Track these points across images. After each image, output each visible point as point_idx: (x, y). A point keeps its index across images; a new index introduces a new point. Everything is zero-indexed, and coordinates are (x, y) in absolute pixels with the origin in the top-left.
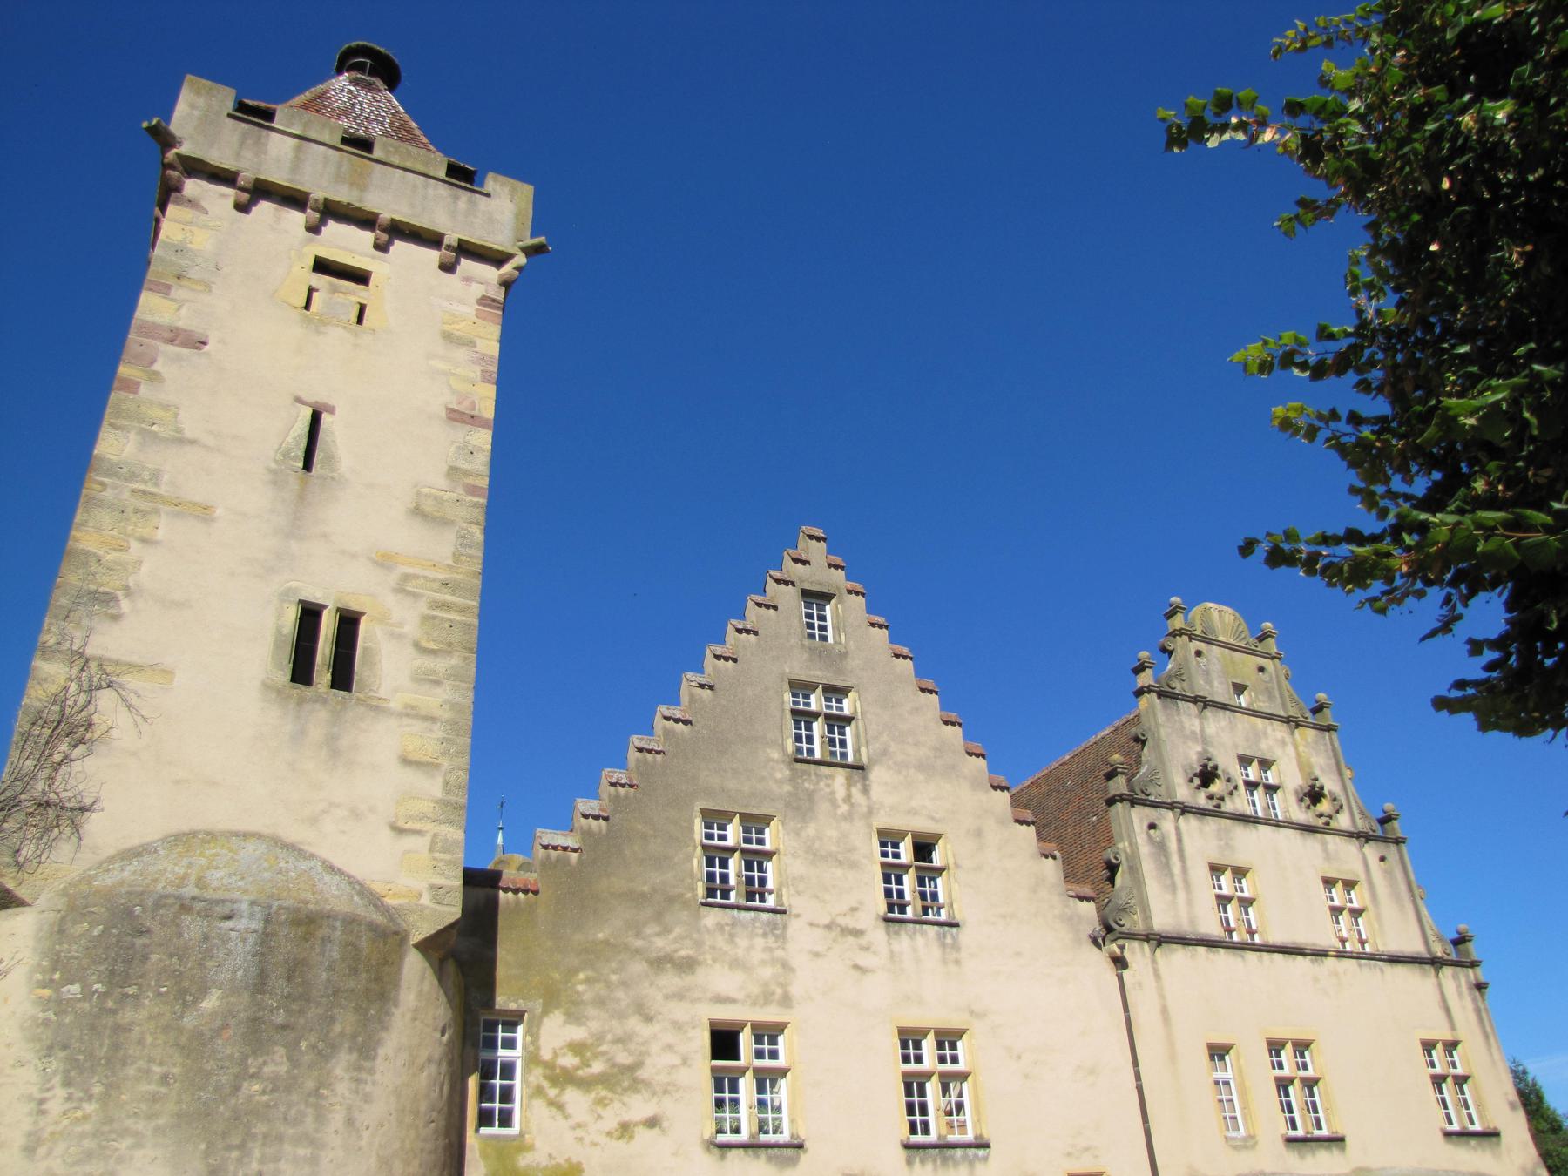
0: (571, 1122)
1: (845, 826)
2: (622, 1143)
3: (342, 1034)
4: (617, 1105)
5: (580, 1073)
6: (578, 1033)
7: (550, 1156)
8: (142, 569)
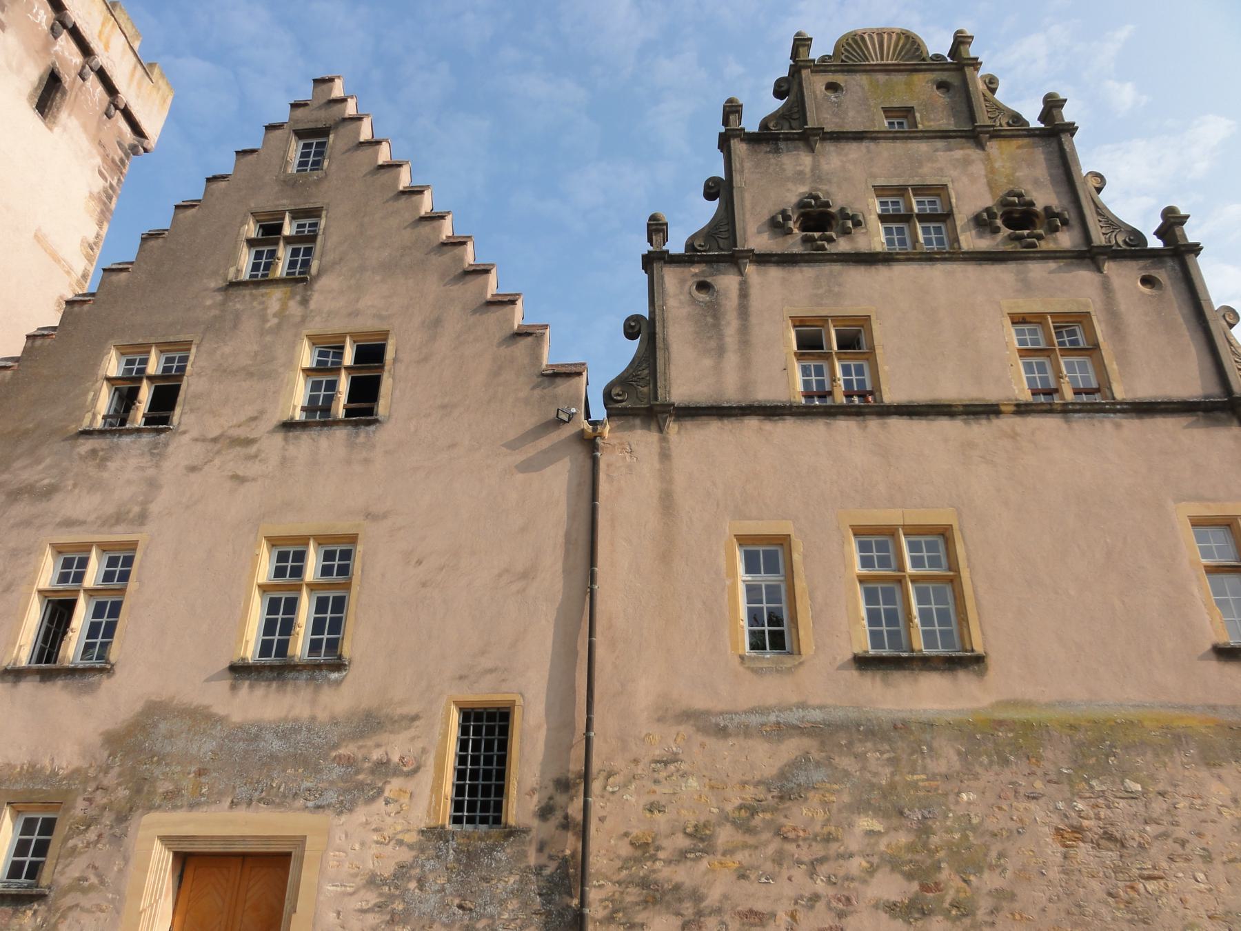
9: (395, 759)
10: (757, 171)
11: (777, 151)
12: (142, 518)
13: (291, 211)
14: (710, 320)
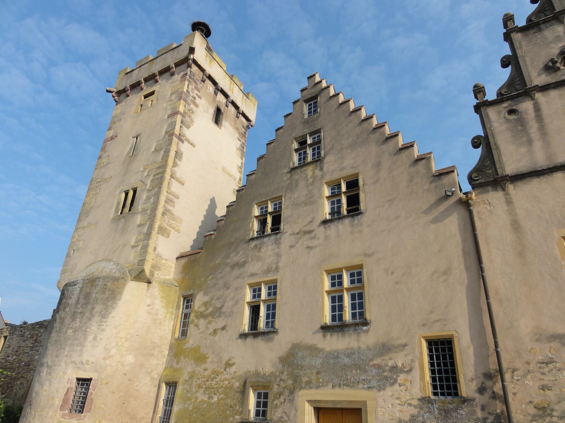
3: (97, 312)
4: (214, 323)
8: (117, 201)
9: (400, 365)
10: (530, 44)
11: (540, 30)
12: (277, 270)
13: (309, 133)
14: (520, 128)
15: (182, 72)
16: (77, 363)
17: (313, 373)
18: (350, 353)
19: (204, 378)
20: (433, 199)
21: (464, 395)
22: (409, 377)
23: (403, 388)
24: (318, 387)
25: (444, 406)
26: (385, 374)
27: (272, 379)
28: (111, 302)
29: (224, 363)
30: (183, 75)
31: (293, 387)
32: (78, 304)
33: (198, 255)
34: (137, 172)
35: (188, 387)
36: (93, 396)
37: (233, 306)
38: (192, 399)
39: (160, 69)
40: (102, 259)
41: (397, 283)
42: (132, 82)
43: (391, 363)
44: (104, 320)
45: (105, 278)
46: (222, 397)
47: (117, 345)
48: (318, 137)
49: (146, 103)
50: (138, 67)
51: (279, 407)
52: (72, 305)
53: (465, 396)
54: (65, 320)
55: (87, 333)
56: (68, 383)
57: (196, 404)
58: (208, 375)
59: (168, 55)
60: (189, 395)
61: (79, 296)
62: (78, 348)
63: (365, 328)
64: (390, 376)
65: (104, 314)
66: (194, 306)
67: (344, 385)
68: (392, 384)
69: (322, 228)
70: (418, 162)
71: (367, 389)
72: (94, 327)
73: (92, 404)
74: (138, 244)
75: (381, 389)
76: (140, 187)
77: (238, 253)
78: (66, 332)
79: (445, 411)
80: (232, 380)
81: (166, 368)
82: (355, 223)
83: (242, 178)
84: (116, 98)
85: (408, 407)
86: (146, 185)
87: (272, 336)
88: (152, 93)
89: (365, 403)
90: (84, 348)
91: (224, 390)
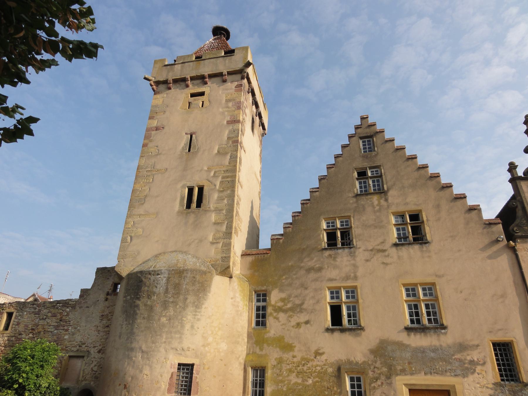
0: (281, 323)
1: (378, 214)
2: (297, 329)
3: (190, 302)
4: (295, 317)
5: (284, 308)
6: (283, 295)
7: (274, 334)
9: (476, 359)
15: (236, 81)
16: (178, 350)
17: (406, 363)
18: (435, 350)
19: (294, 364)
20: (487, 241)
21: (525, 381)
22: (484, 368)
23: (480, 376)
24: (412, 374)
25: (512, 389)
26: (466, 365)
27: (366, 366)
28: (202, 294)
29: (314, 352)
30: (237, 85)
31: (389, 374)
32: (168, 294)
33: (266, 255)
34: (201, 170)
35: (278, 371)
36: (198, 380)
37: (314, 304)
38: (284, 381)
39: (211, 73)
40: (173, 250)
41: (465, 300)
42: (176, 77)
43: (469, 358)
44: (198, 310)
45: (192, 271)
46: (317, 380)
47: (212, 333)
48: (376, 171)
49: (195, 102)
50: (180, 62)
51: (377, 389)
52: (159, 293)
53: (526, 382)
54: (155, 308)
55: (184, 322)
56: (171, 368)
57: (290, 386)
58: (297, 361)
59: (218, 61)
60: (281, 378)
61: (167, 285)
62: (177, 336)
63: (443, 331)
64: (470, 367)
65: (197, 305)
66: (270, 301)
67: (434, 373)
68: (473, 373)
69: (394, 249)
70: (472, 211)
71: (454, 376)
72: (189, 315)
73: (198, 387)
74: (218, 241)
75: (465, 377)
76: (207, 186)
77: (312, 259)
78: (159, 320)
79: (513, 391)
80: (324, 366)
81: (248, 354)
82: (423, 249)
83: (26, 123)
84: (154, 87)
85: (486, 389)
86: (215, 185)
87: (359, 332)
88: (202, 94)
89: (454, 386)
90: (183, 336)
91: (318, 374)
